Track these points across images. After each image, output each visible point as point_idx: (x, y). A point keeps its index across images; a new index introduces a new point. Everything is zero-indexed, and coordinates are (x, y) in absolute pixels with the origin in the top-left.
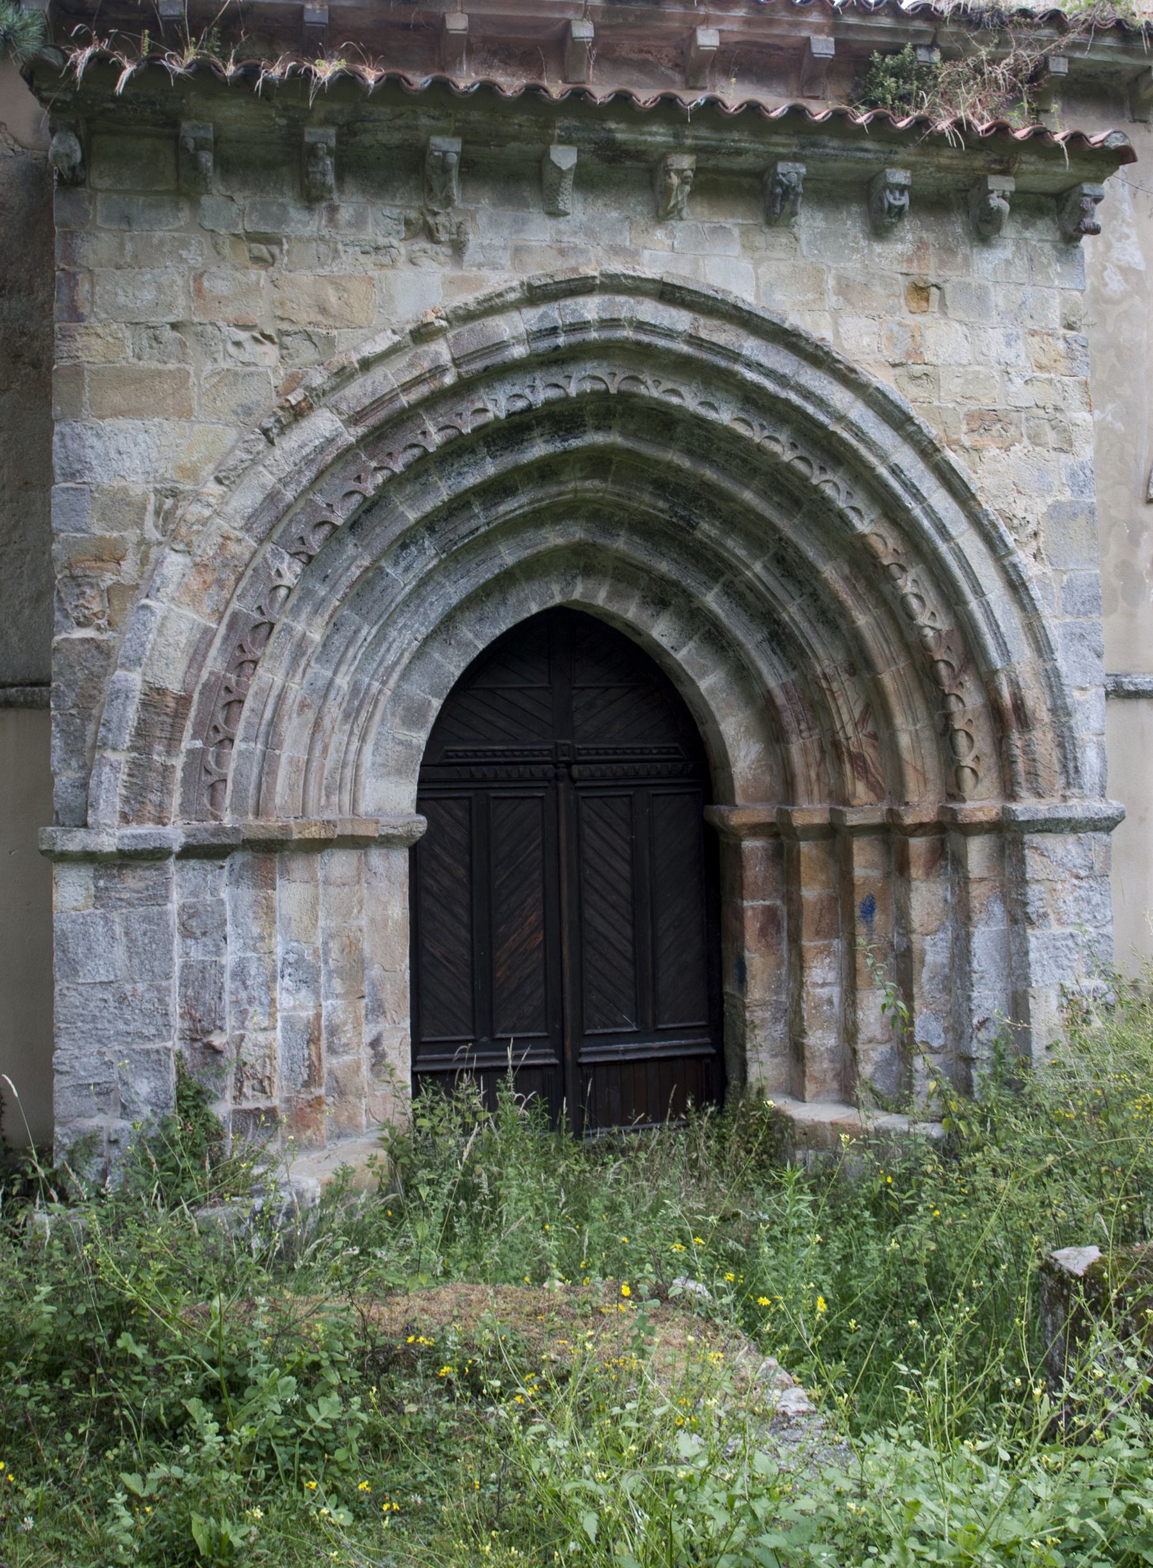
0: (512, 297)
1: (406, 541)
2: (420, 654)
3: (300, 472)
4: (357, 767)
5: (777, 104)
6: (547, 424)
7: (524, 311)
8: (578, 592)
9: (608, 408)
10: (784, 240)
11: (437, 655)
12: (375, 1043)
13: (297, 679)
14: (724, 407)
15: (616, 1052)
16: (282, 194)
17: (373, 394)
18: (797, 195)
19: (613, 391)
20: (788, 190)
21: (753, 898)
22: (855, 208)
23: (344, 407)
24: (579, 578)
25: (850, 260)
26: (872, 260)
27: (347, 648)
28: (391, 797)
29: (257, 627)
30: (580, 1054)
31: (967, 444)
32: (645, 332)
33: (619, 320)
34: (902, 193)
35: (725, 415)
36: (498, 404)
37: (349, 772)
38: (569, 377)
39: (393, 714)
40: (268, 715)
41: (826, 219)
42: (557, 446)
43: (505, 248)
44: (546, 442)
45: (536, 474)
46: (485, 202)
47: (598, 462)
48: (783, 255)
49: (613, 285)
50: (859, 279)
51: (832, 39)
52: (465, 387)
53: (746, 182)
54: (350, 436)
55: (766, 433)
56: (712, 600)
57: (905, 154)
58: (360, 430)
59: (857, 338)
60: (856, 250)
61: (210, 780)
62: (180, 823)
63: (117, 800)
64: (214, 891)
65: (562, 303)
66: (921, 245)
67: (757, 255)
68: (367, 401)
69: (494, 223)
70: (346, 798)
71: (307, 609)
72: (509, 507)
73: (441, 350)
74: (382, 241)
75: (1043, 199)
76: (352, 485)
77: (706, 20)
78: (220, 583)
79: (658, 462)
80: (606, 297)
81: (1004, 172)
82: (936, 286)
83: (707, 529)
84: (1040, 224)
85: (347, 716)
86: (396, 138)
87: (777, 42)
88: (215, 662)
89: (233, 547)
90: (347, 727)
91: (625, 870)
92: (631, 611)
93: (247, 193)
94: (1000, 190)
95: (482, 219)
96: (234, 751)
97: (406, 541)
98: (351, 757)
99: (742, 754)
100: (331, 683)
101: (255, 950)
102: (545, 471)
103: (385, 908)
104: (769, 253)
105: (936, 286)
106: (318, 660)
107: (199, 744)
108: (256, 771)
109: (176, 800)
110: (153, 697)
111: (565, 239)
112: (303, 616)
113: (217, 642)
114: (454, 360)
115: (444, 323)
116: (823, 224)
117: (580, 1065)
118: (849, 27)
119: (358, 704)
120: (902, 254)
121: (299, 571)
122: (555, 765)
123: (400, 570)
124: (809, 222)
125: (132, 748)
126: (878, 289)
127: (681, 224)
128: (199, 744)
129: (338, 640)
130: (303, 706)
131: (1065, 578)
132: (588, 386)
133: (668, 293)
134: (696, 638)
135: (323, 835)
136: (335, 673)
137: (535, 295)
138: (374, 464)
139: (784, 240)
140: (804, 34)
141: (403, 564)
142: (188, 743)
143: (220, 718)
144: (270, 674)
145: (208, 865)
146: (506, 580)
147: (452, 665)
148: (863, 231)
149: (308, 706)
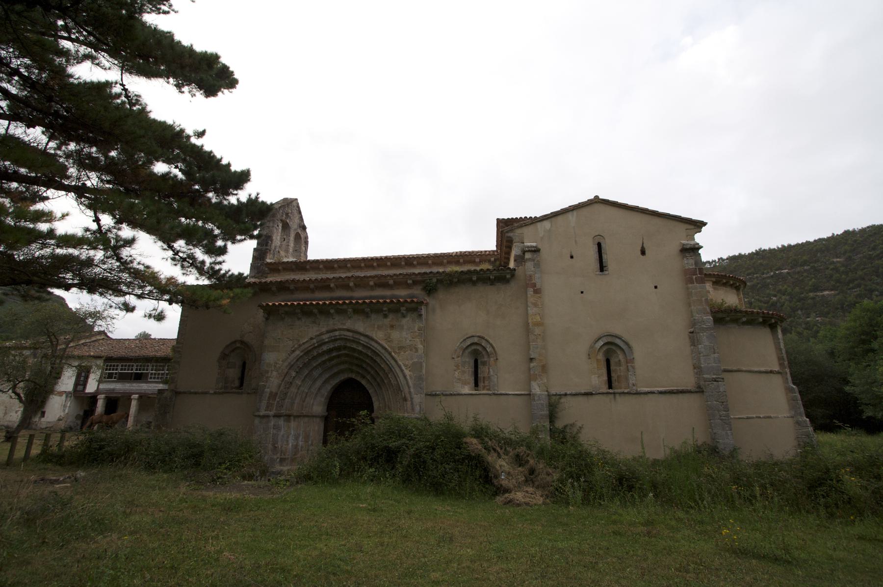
1: (316, 367)
28: (318, 407)
35: (360, 348)
36: (325, 348)
47: (347, 355)
49: (340, 329)
52: (320, 345)
59: (379, 336)
72: (333, 362)
73: (315, 341)
92: (358, 379)
94: (403, 309)
97: (316, 367)
102: (338, 356)
110: (271, 393)
124: (373, 316)
133: (348, 330)
137: (328, 332)
142: (277, 400)
144: (293, 390)
146: (338, 373)
147: (329, 387)
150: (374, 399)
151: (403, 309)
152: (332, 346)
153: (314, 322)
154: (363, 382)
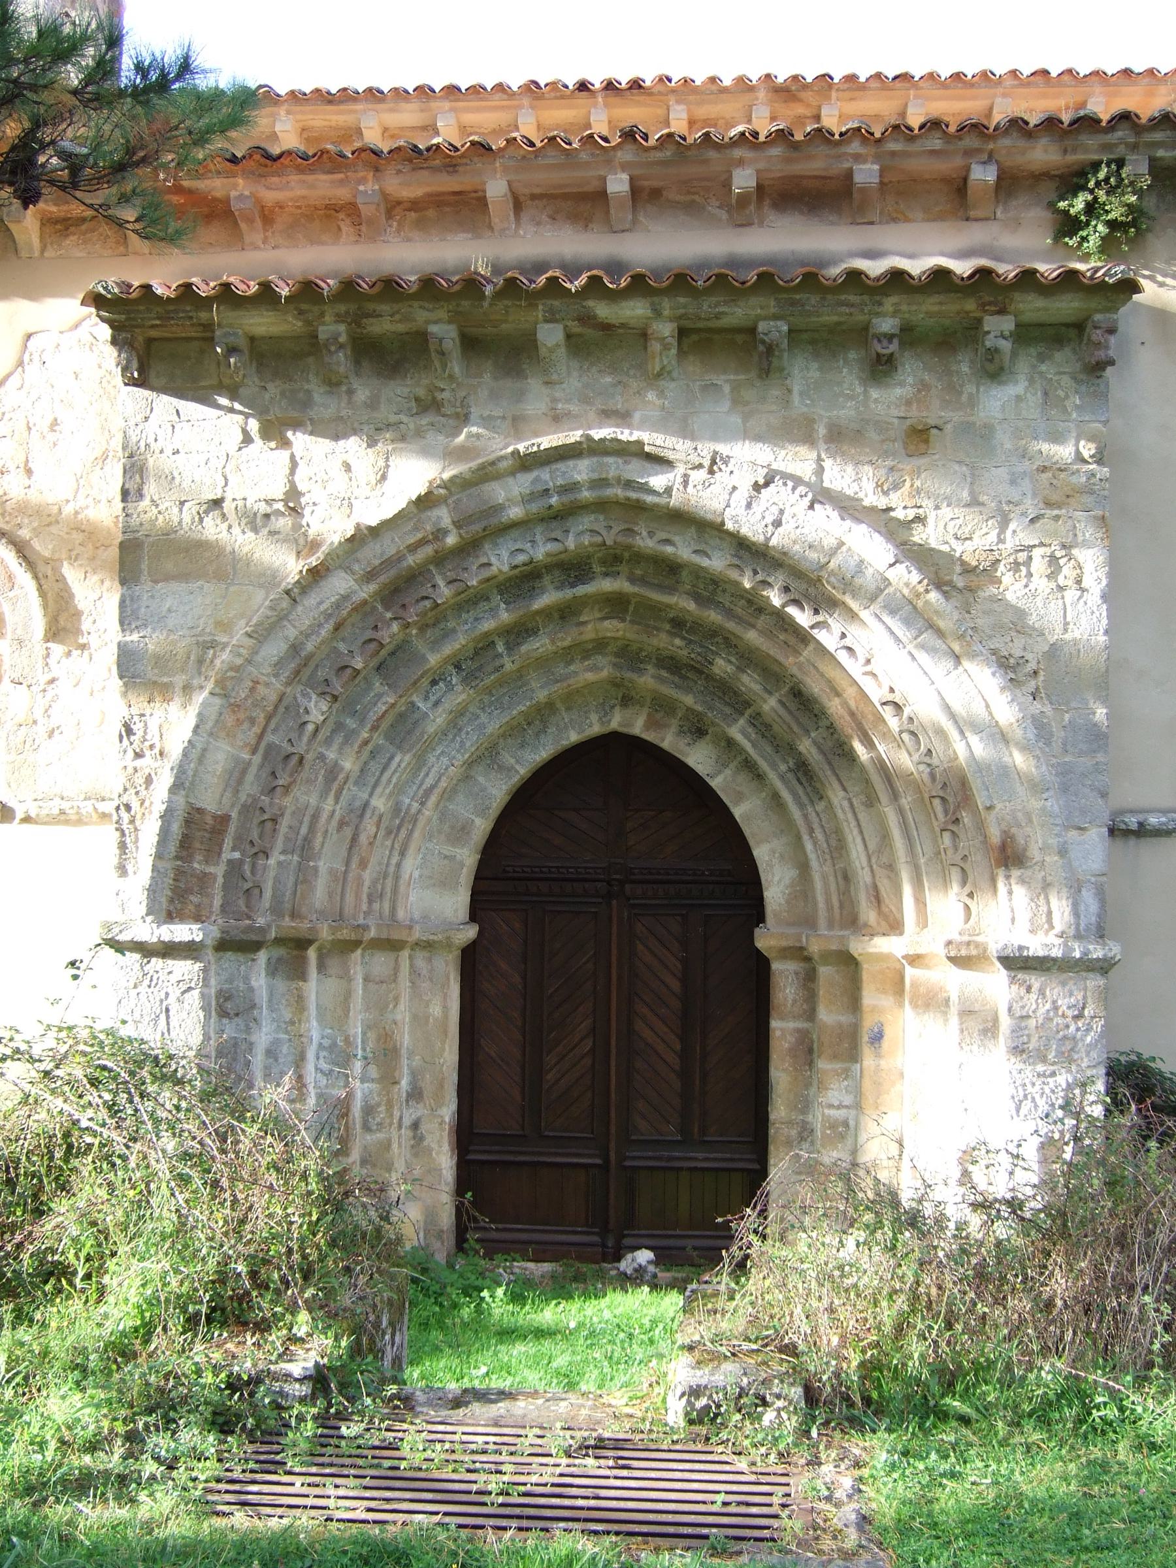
0: (504, 465)
2: (467, 778)
3: (320, 625)
4: (397, 877)
6: (557, 573)
7: (518, 475)
8: (616, 722)
9: (615, 559)
10: (777, 393)
11: (481, 779)
12: (415, 1126)
13: (331, 800)
14: (716, 555)
15: (696, 1159)
16: (308, 381)
17: (382, 554)
18: (782, 351)
19: (609, 542)
20: (770, 349)
21: (782, 1019)
22: (852, 355)
23: (356, 567)
24: (617, 708)
27: (382, 773)
28: (436, 896)
29: (288, 757)
30: (626, 1158)
31: (960, 584)
32: (634, 489)
33: (606, 479)
34: (890, 342)
36: (501, 559)
37: (389, 882)
38: (567, 531)
39: (440, 832)
40: (304, 830)
41: (820, 369)
42: (568, 593)
43: (504, 418)
44: (557, 588)
45: (556, 615)
46: (487, 377)
47: (616, 605)
48: (774, 408)
51: (876, 167)
53: (740, 338)
54: (366, 592)
55: (759, 577)
56: (737, 731)
57: (889, 303)
58: (372, 587)
60: (851, 398)
61: (246, 886)
62: (220, 921)
63: (164, 900)
64: (247, 979)
65: (554, 467)
66: (923, 387)
68: (377, 562)
69: (494, 396)
70: (386, 905)
71: (338, 740)
74: (393, 418)
76: (369, 634)
77: (741, 162)
78: (252, 720)
79: (669, 606)
80: (595, 459)
81: (1002, 311)
83: (722, 666)
84: (1058, 356)
85: (389, 832)
86: (401, 328)
88: (250, 787)
89: (262, 690)
90: (388, 843)
91: (676, 985)
92: (668, 740)
93: (278, 382)
94: (997, 327)
95: (483, 393)
96: (272, 861)
98: (392, 869)
99: (776, 879)
100: (366, 805)
101: (287, 1032)
102: (565, 613)
103: (427, 1006)
106: (356, 783)
107: (237, 855)
108: (292, 879)
109: (217, 902)
111: (560, 406)
112: (335, 746)
113: (253, 770)
114: (454, 522)
115: (442, 491)
116: (818, 374)
117: (626, 1168)
118: (893, 154)
119: (400, 823)
121: (325, 708)
122: (609, 883)
123: (429, 705)
124: (802, 372)
125: (177, 858)
126: (873, 435)
127: (673, 385)
128: (237, 855)
129: (375, 767)
130: (342, 824)
131: (1067, 717)
132: (586, 540)
134: (732, 766)
135: (353, 937)
136: (371, 795)
138: (389, 615)
139: (776, 392)
140: (847, 165)
141: (433, 698)
143: (255, 835)
145: (241, 957)
146: (543, 714)
147: (497, 791)
148: (860, 378)
149: (347, 824)
150: (761, 853)
151: (997, 327)
152: (541, 551)
153: (428, 405)
154: (699, 758)
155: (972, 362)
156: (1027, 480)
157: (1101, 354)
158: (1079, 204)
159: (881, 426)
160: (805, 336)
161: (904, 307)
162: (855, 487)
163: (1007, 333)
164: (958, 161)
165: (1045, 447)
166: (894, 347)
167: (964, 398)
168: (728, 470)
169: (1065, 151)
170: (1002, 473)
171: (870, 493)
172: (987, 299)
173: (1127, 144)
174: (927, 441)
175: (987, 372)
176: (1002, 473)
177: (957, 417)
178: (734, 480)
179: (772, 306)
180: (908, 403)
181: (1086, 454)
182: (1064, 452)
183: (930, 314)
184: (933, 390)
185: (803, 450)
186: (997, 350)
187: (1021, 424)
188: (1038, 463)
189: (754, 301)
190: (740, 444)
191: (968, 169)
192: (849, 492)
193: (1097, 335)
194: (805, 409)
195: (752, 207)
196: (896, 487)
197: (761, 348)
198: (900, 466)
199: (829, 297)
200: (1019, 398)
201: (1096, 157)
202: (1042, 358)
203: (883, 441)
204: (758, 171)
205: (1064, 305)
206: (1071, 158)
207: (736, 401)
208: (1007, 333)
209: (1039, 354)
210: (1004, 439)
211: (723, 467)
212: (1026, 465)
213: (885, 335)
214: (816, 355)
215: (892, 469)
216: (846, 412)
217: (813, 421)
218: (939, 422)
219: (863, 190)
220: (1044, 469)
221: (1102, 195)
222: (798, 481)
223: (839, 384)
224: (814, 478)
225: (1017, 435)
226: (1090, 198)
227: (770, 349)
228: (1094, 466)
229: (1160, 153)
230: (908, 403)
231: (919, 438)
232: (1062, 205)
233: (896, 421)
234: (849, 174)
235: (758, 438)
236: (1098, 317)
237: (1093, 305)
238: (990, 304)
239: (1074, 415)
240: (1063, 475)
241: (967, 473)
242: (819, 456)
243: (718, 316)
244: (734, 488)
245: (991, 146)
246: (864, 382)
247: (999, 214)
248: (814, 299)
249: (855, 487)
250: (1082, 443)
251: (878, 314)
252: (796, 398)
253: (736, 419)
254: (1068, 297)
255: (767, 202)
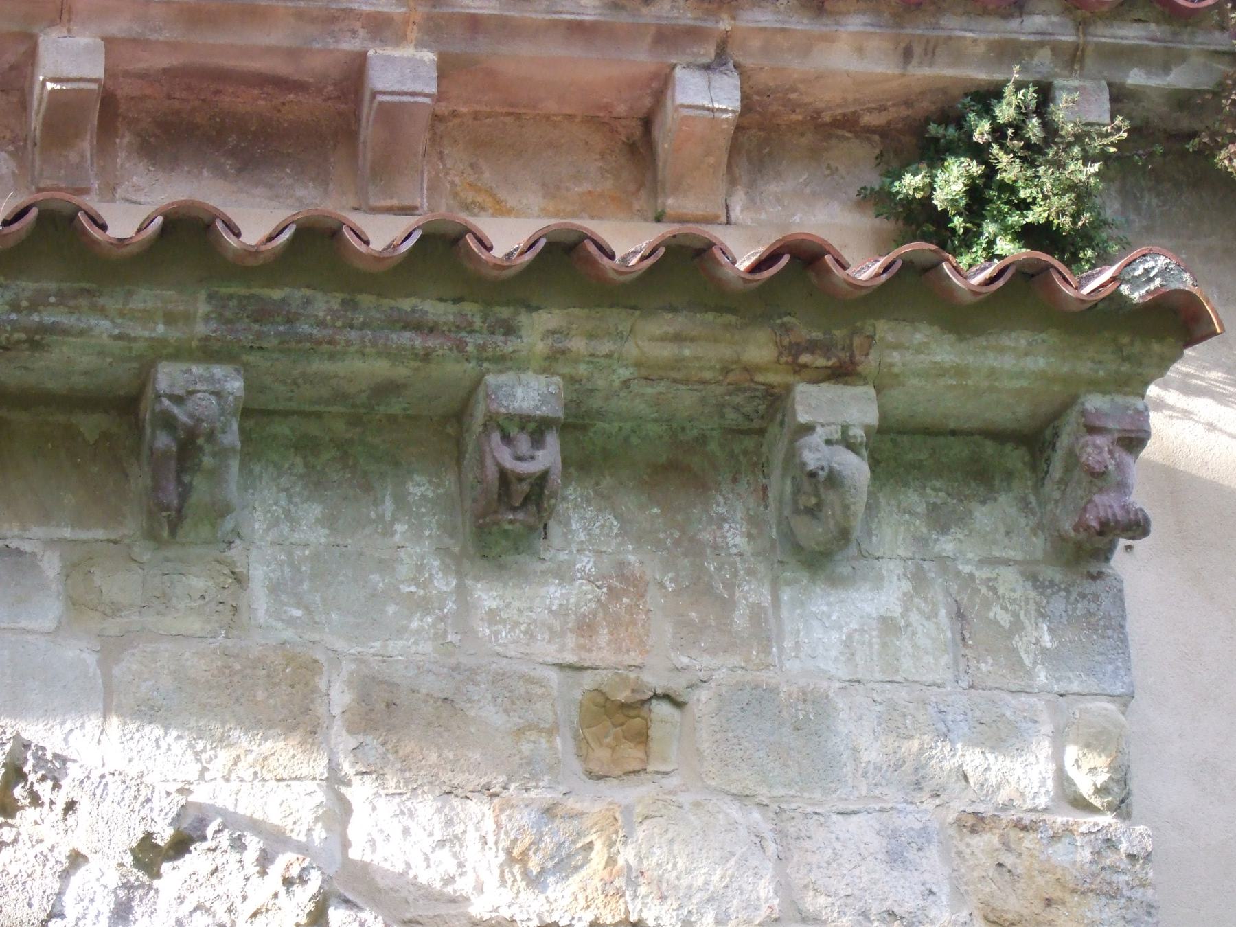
5: (256, 219)
10: (198, 583)
18: (223, 454)
20: (190, 446)
22: (419, 488)
25: (401, 632)
26: (467, 632)
34: (537, 440)
41: (329, 521)
48: (195, 625)
50: (429, 684)
51: (429, 56)
53: (90, 425)
57: (537, 328)
60: (424, 605)
66: (623, 583)
67: (113, 627)
75: (989, 447)
81: (842, 373)
82: (667, 697)
84: (984, 516)
87: (281, 67)
94: (833, 417)
104: (150, 619)
105: (667, 697)
116: (320, 536)
120: (562, 612)
124: (276, 529)
126: (491, 714)
140: (350, 45)
148: (442, 551)
151: (833, 417)
155: (752, 520)
156: (933, 852)
157: (1106, 504)
158: (951, 181)
159: (513, 690)
160: (282, 428)
161: (578, 344)
162: (445, 861)
163: (858, 433)
164: (642, 59)
165: (973, 760)
166: (548, 457)
167: (740, 619)
168: (61, 800)
169: (907, 55)
170: (862, 829)
171: (491, 881)
172: (805, 333)
173: (1056, 49)
174: (642, 738)
175: (798, 548)
176: (861, 830)
177: (722, 667)
178: (80, 834)
179: (200, 315)
180: (586, 627)
181: (1085, 786)
182: (1023, 775)
183: (649, 372)
184: (653, 590)
185: (282, 751)
186: (834, 480)
187: (902, 695)
188: (959, 805)
189: (145, 298)
190: (93, 722)
191: (662, 84)
192: (427, 876)
193: (1097, 450)
194: (288, 634)
195: (86, 145)
196: (565, 863)
197: (163, 441)
198: (572, 803)
199: (366, 300)
200: (888, 626)
201: (982, 76)
202: (941, 520)
203: (520, 732)
204: (110, 42)
205: (1007, 362)
206: (924, 73)
207: (78, 604)
208: (858, 433)
209: (933, 508)
210: (861, 738)
211: (44, 790)
212: (923, 813)
213: (523, 421)
214: (316, 483)
215: (549, 811)
216: (410, 646)
217: (313, 666)
218: (676, 684)
219: (392, 114)
220: (975, 823)
221: (1009, 168)
222: (275, 841)
223: (386, 566)
224: (319, 834)
225: (893, 722)
226: (976, 169)
227: (190, 446)
228: (1107, 819)
229: (1135, 78)
230: (586, 627)
231: (622, 723)
232: (910, 183)
233: (553, 676)
234: (357, 68)
235: (148, 711)
236: (1094, 402)
237: (1084, 368)
238: (812, 347)
239: (1042, 677)
240: (1029, 841)
241: (766, 828)
242: (333, 768)
243: (37, 340)
244: (77, 859)
245: (725, 24)
246: (456, 563)
247: (737, 213)
248: (324, 304)
249: (445, 861)
250: (1072, 752)
251: (502, 361)
252: (259, 599)
253: (79, 654)
254: (1019, 339)
255: (125, 139)
